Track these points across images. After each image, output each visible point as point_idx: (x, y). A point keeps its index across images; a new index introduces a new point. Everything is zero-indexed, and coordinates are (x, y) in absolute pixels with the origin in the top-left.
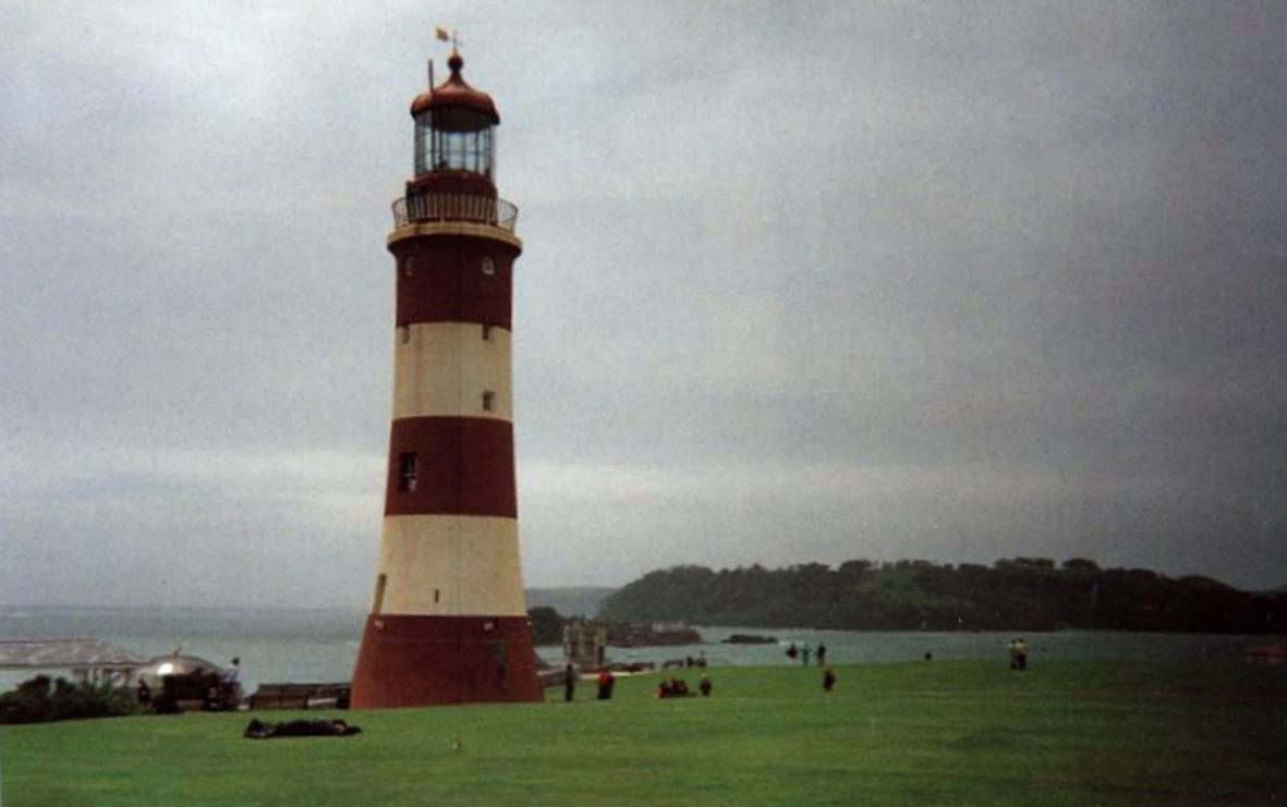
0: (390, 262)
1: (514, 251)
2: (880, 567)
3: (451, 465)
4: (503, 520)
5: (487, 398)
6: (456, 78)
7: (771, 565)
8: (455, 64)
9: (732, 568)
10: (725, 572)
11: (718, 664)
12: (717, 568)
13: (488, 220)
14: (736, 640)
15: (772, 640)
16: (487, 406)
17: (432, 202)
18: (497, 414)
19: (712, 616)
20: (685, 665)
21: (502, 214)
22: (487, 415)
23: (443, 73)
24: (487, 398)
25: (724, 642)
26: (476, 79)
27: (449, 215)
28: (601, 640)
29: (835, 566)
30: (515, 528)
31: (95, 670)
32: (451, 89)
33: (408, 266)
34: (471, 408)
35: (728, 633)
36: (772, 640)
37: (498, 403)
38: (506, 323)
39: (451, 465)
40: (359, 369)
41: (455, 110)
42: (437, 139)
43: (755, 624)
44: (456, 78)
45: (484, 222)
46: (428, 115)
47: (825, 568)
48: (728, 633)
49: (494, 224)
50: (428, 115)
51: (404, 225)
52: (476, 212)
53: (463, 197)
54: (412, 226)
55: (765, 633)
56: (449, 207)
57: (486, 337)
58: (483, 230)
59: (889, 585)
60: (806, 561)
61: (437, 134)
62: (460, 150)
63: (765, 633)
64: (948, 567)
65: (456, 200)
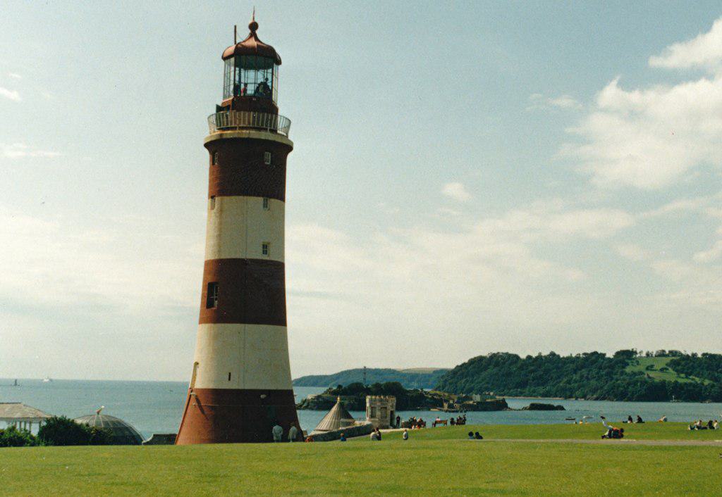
0: (206, 152)
1: (289, 148)
2: (644, 355)
3: (245, 291)
4: (279, 327)
5: (265, 248)
6: (253, 35)
7: (563, 354)
8: (254, 27)
9: (534, 355)
10: (529, 357)
11: (654, 419)
12: (523, 356)
13: (269, 128)
14: (534, 407)
15: (561, 408)
16: (265, 252)
17: (244, 117)
18: (272, 257)
19: (520, 388)
20: (449, 423)
21: (281, 124)
22: (265, 257)
23: (244, 33)
24: (265, 248)
25: (525, 409)
26: (265, 37)
27: (241, 125)
28: (392, 406)
29: (610, 355)
30: (286, 330)
31: (20, 423)
32: (252, 42)
33: (216, 158)
34: (255, 254)
35: (527, 403)
36: (561, 408)
37: (271, 250)
38: (281, 196)
39: (245, 291)
40: (180, 238)
41: (254, 56)
42: (237, 72)
43: (545, 395)
44: (253, 35)
45: (266, 129)
46: (233, 60)
47: (517, 357)
48: (527, 403)
49: (274, 131)
50: (233, 60)
51: (214, 132)
52: (237, 123)
53: (242, 113)
54: (219, 132)
55: (555, 402)
56: (225, 122)
57: (265, 205)
58: (270, 137)
59: (650, 368)
60: (512, 352)
61: (237, 69)
62: (252, 79)
63: (555, 402)
64: (694, 355)
65: (243, 71)
